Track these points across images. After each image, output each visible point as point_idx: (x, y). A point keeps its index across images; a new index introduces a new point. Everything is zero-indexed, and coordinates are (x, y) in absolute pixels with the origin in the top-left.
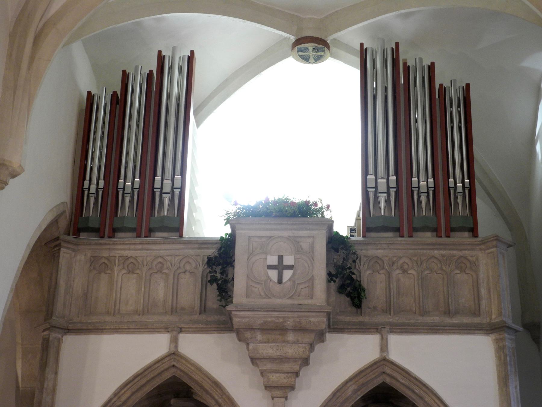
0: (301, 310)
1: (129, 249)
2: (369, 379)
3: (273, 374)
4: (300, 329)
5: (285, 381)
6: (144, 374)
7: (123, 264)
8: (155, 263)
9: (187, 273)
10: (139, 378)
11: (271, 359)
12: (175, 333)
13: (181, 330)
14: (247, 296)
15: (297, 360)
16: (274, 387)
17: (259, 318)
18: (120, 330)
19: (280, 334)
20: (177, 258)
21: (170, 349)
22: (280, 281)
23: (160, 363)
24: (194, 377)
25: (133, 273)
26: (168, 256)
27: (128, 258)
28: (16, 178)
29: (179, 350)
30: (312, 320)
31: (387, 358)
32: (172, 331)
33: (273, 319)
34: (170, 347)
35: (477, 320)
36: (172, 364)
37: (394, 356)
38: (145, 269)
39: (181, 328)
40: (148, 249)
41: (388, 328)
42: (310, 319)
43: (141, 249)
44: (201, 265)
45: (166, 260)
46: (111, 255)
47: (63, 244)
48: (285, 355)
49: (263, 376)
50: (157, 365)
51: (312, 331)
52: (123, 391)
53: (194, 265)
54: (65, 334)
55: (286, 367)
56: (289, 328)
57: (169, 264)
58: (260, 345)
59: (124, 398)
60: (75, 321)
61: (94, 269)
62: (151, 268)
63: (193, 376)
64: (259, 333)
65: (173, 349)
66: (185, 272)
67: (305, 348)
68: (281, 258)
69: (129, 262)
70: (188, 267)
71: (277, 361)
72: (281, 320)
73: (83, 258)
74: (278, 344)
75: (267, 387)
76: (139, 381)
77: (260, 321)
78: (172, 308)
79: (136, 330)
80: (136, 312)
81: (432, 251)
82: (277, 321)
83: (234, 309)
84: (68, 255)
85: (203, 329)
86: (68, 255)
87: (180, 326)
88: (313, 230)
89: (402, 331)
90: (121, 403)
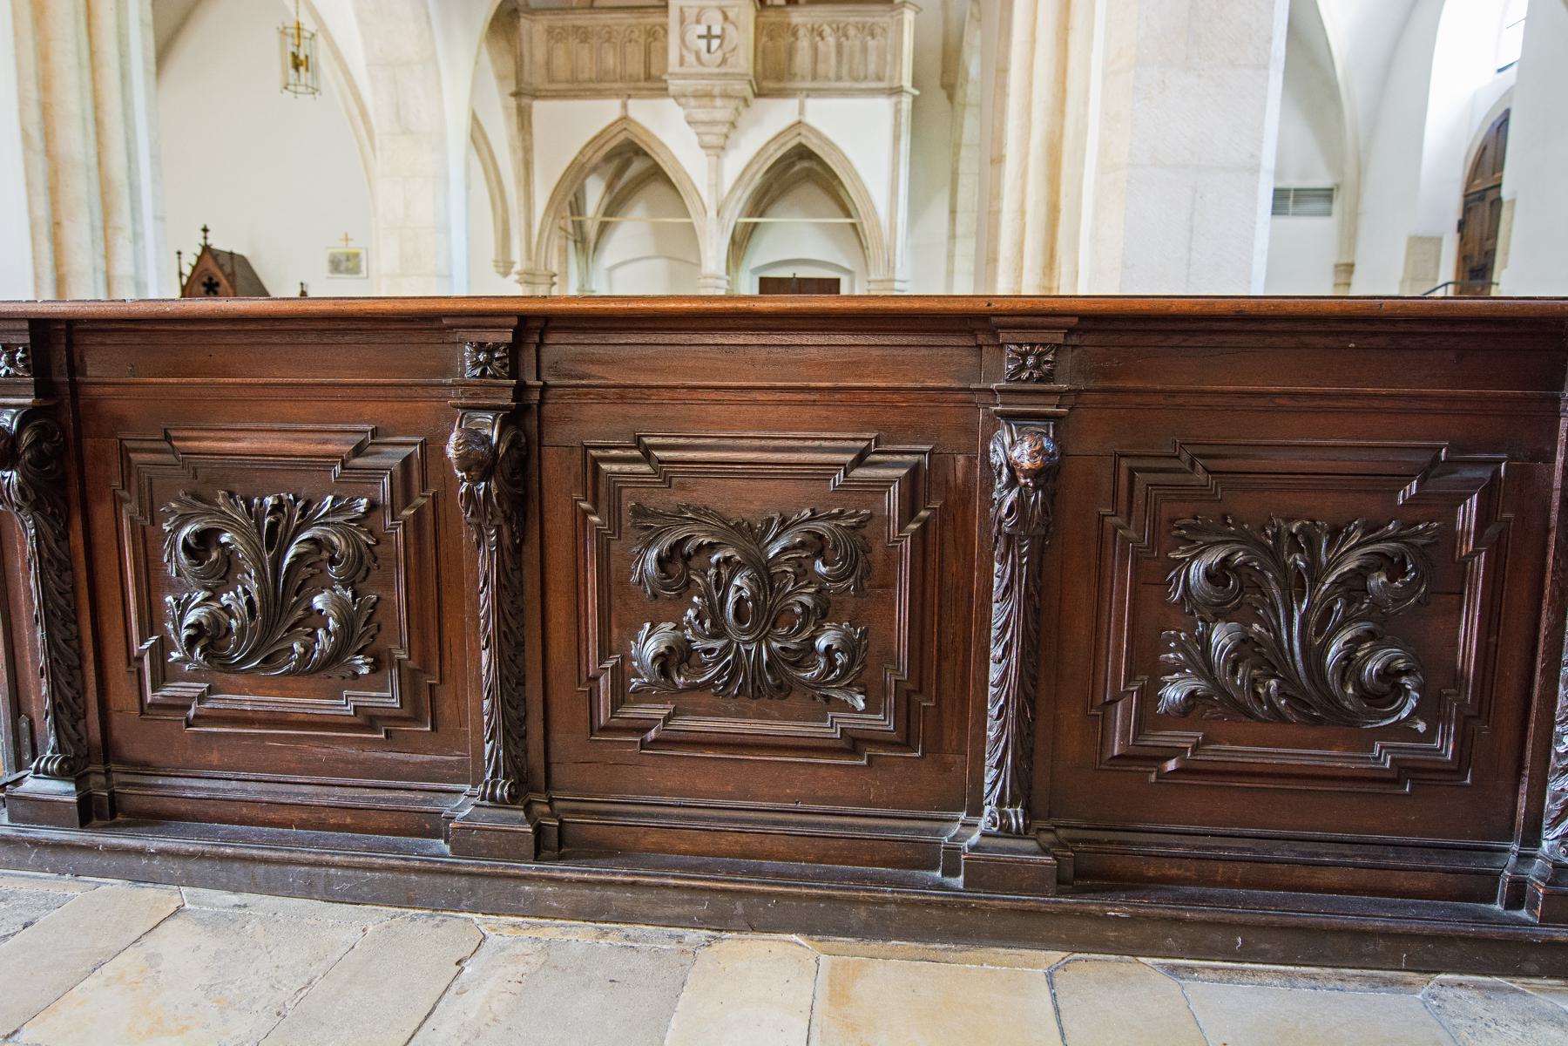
4: (726, 96)
8: (604, 32)
13: (629, 96)
17: (692, 85)
22: (709, 51)
35: (881, 85)
37: (810, 119)
38: (595, 39)
41: (805, 93)
47: (522, 15)
55: (717, 129)
59: (587, 157)
61: (552, 38)
68: (709, 28)
69: (580, 31)
75: (703, 147)
77: (691, 89)
80: (591, 80)
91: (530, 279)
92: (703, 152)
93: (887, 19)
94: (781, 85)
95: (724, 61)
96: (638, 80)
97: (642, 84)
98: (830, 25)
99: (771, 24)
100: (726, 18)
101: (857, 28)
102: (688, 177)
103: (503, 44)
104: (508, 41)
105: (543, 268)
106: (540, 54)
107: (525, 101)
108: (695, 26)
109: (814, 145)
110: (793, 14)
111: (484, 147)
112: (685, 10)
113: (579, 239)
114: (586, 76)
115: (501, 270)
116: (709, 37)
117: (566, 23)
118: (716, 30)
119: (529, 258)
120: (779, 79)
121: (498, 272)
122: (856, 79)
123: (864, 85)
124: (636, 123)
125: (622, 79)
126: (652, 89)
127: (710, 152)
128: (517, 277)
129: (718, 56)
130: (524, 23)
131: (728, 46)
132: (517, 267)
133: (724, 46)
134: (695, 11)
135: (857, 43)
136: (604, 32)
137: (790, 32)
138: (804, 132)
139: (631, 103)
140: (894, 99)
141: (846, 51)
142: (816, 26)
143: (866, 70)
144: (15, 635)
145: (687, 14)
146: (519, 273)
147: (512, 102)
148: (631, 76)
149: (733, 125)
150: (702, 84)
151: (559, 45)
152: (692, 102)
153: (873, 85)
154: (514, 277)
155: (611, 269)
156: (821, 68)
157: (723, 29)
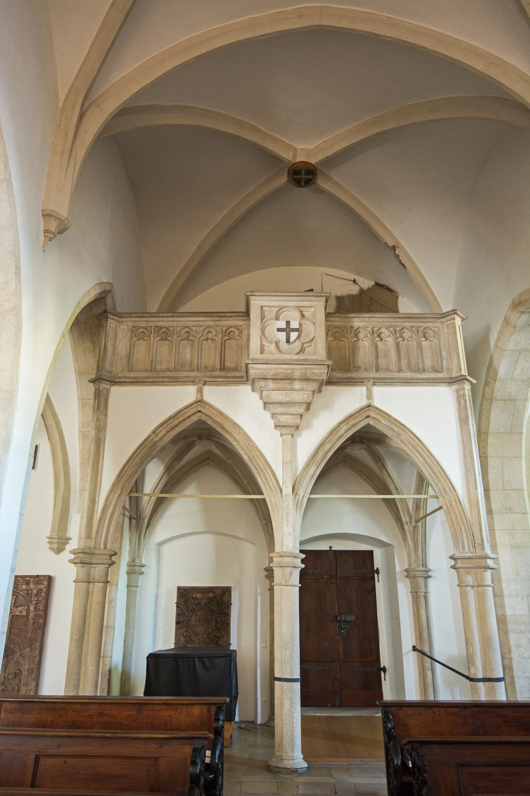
0: (307, 363)
1: (163, 321)
2: (357, 421)
3: (282, 416)
4: (305, 379)
5: (292, 421)
6: (176, 417)
7: (158, 332)
8: (183, 332)
9: (209, 340)
10: (172, 420)
11: (281, 403)
12: (200, 385)
13: (205, 383)
14: (262, 353)
15: (302, 404)
16: (283, 426)
17: (272, 369)
18: (156, 383)
19: (288, 383)
20: (201, 328)
21: (197, 397)
22: (288, 341)
23: (189, 408)
24: (217, 420)
25: (166, 340)
26: (194, 326)
27: (161, 328)
28: (66, 233)
29: (204, 399)
30: (316, 371)
31: (372, 404)
32: (198, 383)
33: (283, 371)
34: (197, 396)
35: (440, 375)
36: (199, 409)
37: (377, 403)
38: (175, 336)
39: (205, 382)
40: (177, 321)
41: (372, 381)
42: (314, 371)
43: (173, 321)
44: (220, 333)
45: (192, 330)
46: (148, 325)
47: (110, 316)
48: (292, 400)
49: (272, 418)
50: (187, 410)
51: (315, 380)
52: (159, 430)
53: (214, 333)
54: (113, 385)
55: (293, 410)
56: (296, 377)
57: (194, 332)
58: (273, 392)
59: (160, 436)
60: (120, 375)
61: (135, 336)
62: (180, 336)
63: (215, 419)
64: (271, 382)
65: (199, 398)
66: (207, 339)
67: (309, 395)
68: (288, 323)
69: (163, 331)
70: (210, 336)
71: (286, 405)
72: (290, 372)
73: (126, 327)
74: (287, 392)
75: (276, 426)
76: (172, 422)
77: (272, 373)
78: (198, 366)
79: (170, 383)
80: (168, 370)
81: (403, 323)
82: (287, 372)
83: (251, 362)
84: (114, 325)
85: (222, 383)
86: (114, 325)
87: (205, 380)
88: (314, 301)
89: (383, 384)
90: (158, 439)
91: (87, 558)
92: (277, 433)
93: (438, 324)
94: (349, 375)
95: (302, 351)
96: (214, 370)
97: (217, 373)
98: (388, 328)
99: (335, 327)
100: (303, 316)
101: (411, 331)
102: (262, 455)
103: (88, 344)
104: (93, 343)
105: (102, 547)
106: (122, 348)
107: (104, 386)
108: (274, 321)
109: (382, 426)
110: (355, 320)
111: (54, 428)
112: (264, 309)
113: (135, 516)
114: (164, 367)
115: (55, 546)
116: (288, 329)
117: (149, 324)
118: (294, 325)
119: (89, 536)
120: (349, 370)
121: (51, 549)
122: (418, 370)
123: (424, 376)
124: (211, 406)
125: (198, 369)
126: (226, 377)
127: (285, 431)
128: (72, 556)
129: (297, 346)
130: (111, 323)
131: (303, 339)
132: (73, 545)
133: (301, 338)
134: (275, 310)
135: (413, 344)
136: (183, 332)
137: (353, 333)
138: (372, 414)
139: (206, 388)
140: (454, 387)
141: (403, 349)
142: (375, 329)
143: (423, 363)
144: (166, 421)
145: (266, 313)
146: (73, 552)
147: (92, 388)
148: (206, 367)
149: (308, 406)
150: (283, 369)
151: (141, 341)
152: (271, 385)
153: (434, 375)
154: (67, 555)
155: (160, 544)
156: (382, 362)
157: (300, 324)
